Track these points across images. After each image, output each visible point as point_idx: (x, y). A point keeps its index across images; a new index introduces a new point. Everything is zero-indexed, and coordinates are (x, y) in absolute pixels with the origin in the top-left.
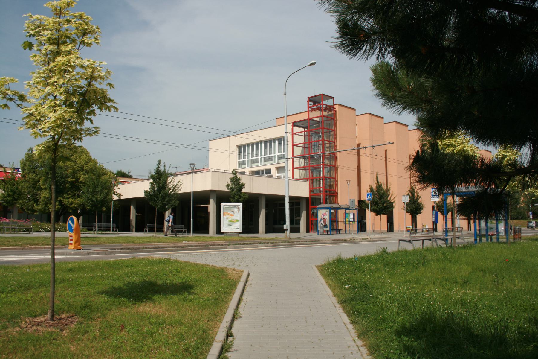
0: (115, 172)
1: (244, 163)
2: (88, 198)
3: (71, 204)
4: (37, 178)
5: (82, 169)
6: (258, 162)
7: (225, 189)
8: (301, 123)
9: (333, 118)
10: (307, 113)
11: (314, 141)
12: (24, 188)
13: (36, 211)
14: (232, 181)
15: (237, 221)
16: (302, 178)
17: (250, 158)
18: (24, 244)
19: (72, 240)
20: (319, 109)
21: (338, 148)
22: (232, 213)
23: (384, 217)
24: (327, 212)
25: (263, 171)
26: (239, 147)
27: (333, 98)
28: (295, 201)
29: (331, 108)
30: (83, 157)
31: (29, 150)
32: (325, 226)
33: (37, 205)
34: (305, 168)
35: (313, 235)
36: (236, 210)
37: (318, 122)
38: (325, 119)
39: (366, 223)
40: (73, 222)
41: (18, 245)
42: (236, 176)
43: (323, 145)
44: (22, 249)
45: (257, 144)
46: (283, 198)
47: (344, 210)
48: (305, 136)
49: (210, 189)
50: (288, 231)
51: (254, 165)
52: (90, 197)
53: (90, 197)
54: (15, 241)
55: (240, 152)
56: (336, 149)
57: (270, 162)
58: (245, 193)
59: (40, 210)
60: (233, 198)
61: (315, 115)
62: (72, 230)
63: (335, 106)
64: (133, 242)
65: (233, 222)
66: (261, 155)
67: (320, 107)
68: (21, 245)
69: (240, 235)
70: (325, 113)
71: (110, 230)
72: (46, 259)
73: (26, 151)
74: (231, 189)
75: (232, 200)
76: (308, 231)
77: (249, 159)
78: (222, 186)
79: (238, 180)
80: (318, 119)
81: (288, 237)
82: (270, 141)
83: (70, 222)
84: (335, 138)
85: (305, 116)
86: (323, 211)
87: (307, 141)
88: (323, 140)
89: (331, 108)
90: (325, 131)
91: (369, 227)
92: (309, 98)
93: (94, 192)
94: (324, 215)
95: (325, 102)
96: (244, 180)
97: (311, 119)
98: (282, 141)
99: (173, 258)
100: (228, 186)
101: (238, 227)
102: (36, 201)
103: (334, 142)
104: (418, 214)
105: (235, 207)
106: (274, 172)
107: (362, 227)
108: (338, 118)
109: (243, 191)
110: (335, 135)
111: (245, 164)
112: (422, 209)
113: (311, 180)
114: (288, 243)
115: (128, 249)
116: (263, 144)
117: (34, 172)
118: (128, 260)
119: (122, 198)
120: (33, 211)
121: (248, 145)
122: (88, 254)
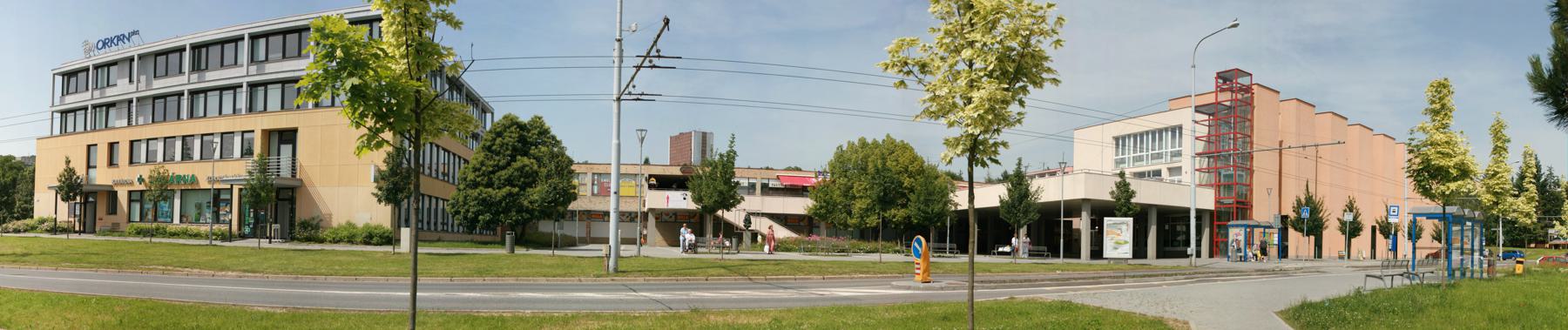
0: (389, 208)
1: (1122, 161)
2: (919, 209)
3: (894, 217)
4: (849, 184)
5: (906, 171)
6: (1162, 158)
7: (1108, 198)
8: (1206, 108)
9: (1249, 103)
10: (1214, 94)
11: (1224, 134)
12: (836, 195)
13: (850, 227)
14: (1118, 187)
15: (1126, 242)
16: (1204, 183)
17: (1132, 155)
18: (852, 272)
19: (919, 269)
20: (1231, 90)
21: (1255, 146)
22: (1119, 232)
23: (1312, 238)
24: (1242, 231)
25: (1149, 172)
26: (1117, 139)
27: (1251, 75)
28: (1200, 213)
29: (1248, 89)
30: (907, 154)
31: (838, 148)
32: (1239, 250)
33: (851, 218)
34: (1208, 171)
35: (1220, 262)
36: (1124, 227)
37: (1230, 107)
38: (1239, 103)
39: (1287, 247)
40: (920, 244)
41: (846, 273)
42: (1124, 180)
43: (1235, 139)
44: (852, 278)
45: (1141, 135)
46: (1187, 211)
47: (1262, 230)
48: (1209, 126)
49: (1083, 197)
50: (1194, 256)
51: (1137, 164)
52: (922, 207)
53: (922, 207)
54: (839, 267)
55: (1117, 145)
56: (1252, 148)
57: (1160, 161)
58: (1136, 204)
59: (855, 224)
60: (1120, 210)
61: (1225, 97)
62: (919, 256)
63: (1253, 87)
64: (990, 271)
65: (1120, 244)
66: (1147, 150)
67: (1232, 88)
68: (849, 273)
69: (1130, 262)
70: (1239, 96)
71: (945, 252)
72: (872, 296)
73: (835, 150)
74: (1118, 199)
75: (1117, 213)
76: (1211, 256)
77: (1130, 155)
78: (1104, 192)
79: (1126, 185)
80: (1228, 103)
81: (1193, 263)
82: (1160, 131)
83: (916, 244)
84: (1252, 130)
85: (1211, 99)
86: (1236, 230)
87: (1213, 133)
88: (1235, 134)
89: (1248, 89)
90: (1238, 120)
91: (1291, 252)
92: (1218, 73)
93: (927, 202)
94: (1237, 235)
95: (1239, 80)
96: (1135, 185)
97: (1218, 103)
98: (1145, 137)
99: (1078, 301)
100: (1112, 193)
101: (1126, 251)
102: (849, 213)
103: (1250, 137)
104: (1355, 236)
105: (1123, 223)
106: (1165, 174)
107: (1283, 252)
108: (1255, 104)
109: (1133, 200)
110: (1252, 127)
111: (1125, 163)
112: (1362, 230)
113: (1217, 186)
114: (1194, 275)
115: (991, 282)
116: (1150, 136)
117: (846, 176)
118: (1003, 302)
119: (959, 208)
120: (846, 226)
121: (1129, 136)
122: (942, 289)
